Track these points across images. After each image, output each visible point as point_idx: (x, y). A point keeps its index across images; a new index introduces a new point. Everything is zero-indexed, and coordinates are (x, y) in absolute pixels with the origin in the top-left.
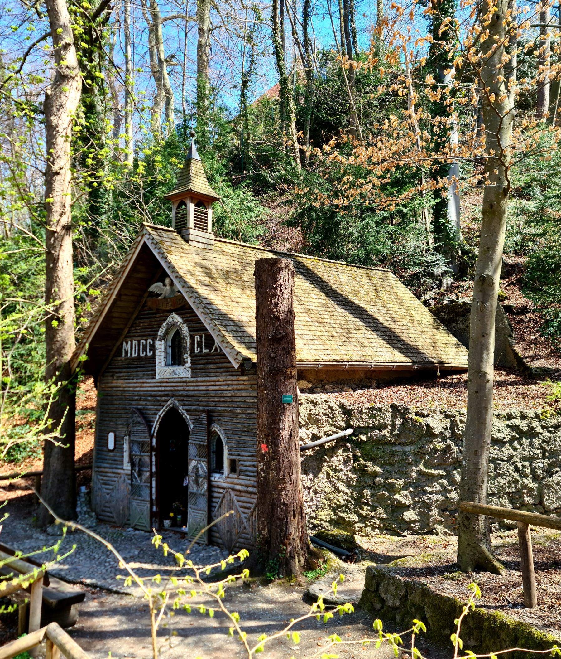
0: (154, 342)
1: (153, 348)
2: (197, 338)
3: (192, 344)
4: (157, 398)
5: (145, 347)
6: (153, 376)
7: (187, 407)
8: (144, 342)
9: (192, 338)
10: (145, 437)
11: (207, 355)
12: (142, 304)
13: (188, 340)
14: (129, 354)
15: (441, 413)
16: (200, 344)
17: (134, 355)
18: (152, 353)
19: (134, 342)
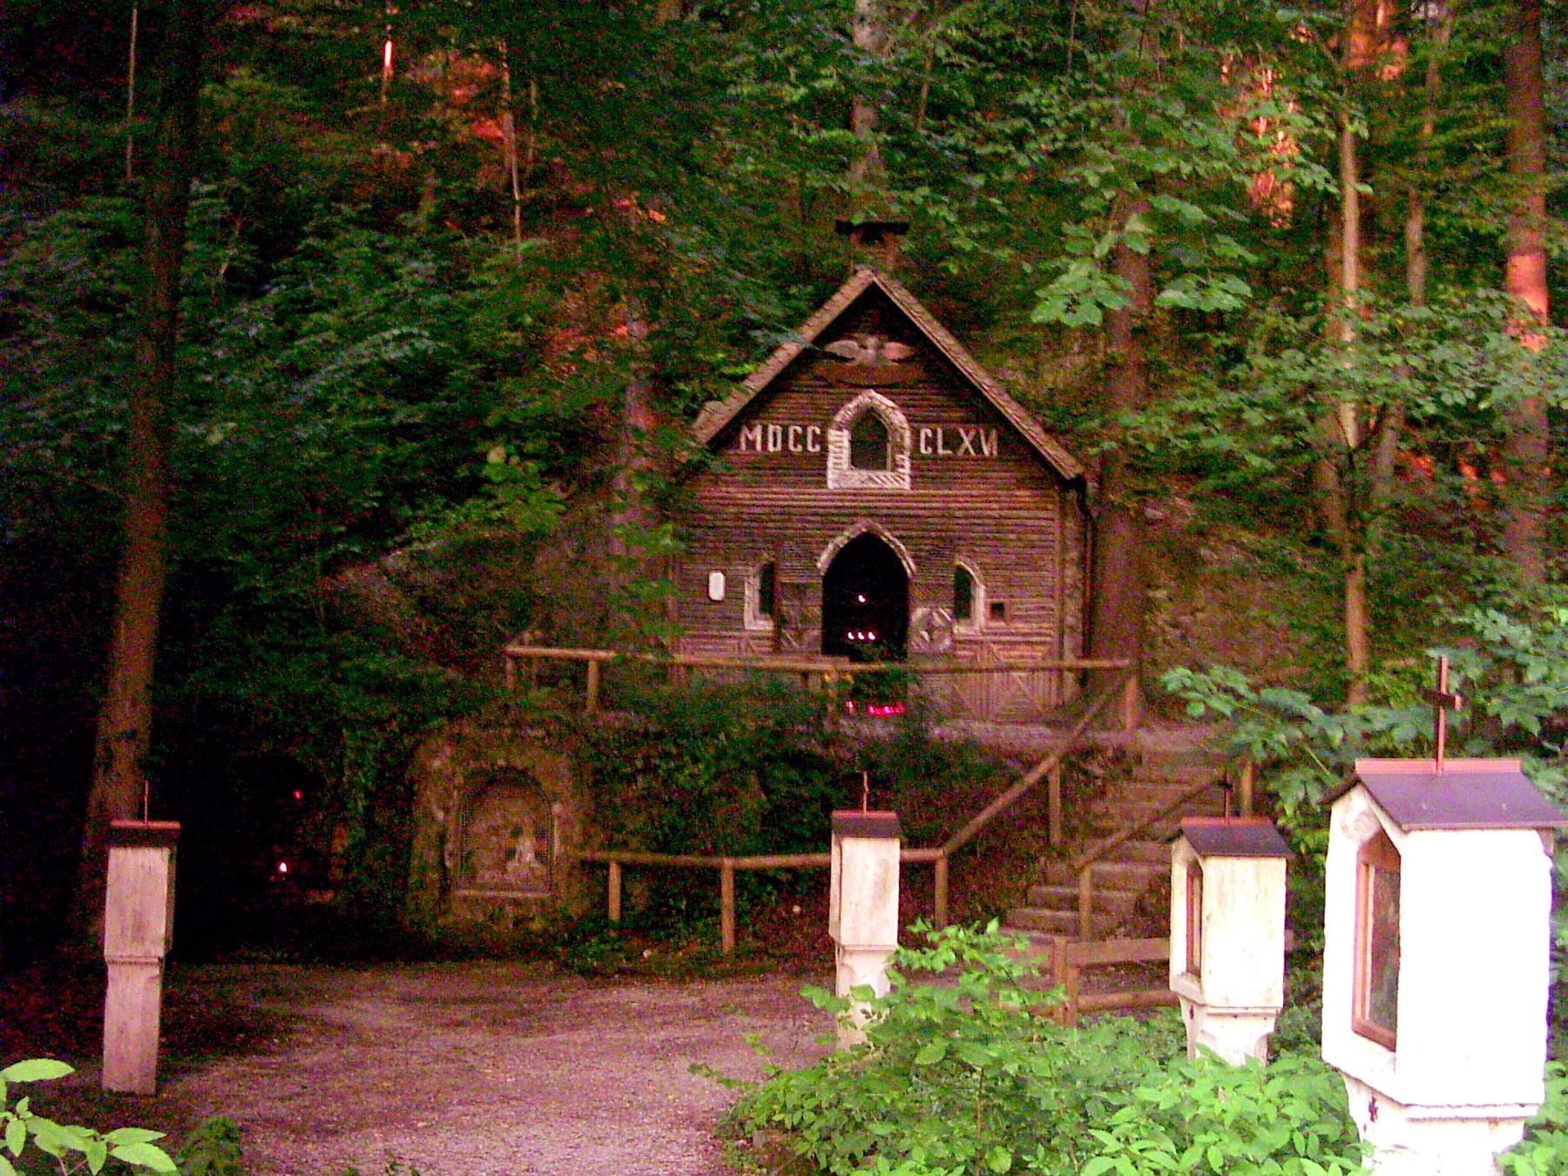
0: (824, 432)
1: (821, 440)
2: (925, 432)
3: (916, 442)
4: (830, 520)
5: (800, 439)
6: (823, 483)
7: (897, 533)
8: (799, 429)
9: (916, 433)
10: (566, 840)
11: (943, 459)
12: (739, 371)
13: (907, 434)
14: (759, 447)
15: (1149, 395)
16: (931, 442)
17: (771, 448)
18: (818, 448)
19: (771, 428)
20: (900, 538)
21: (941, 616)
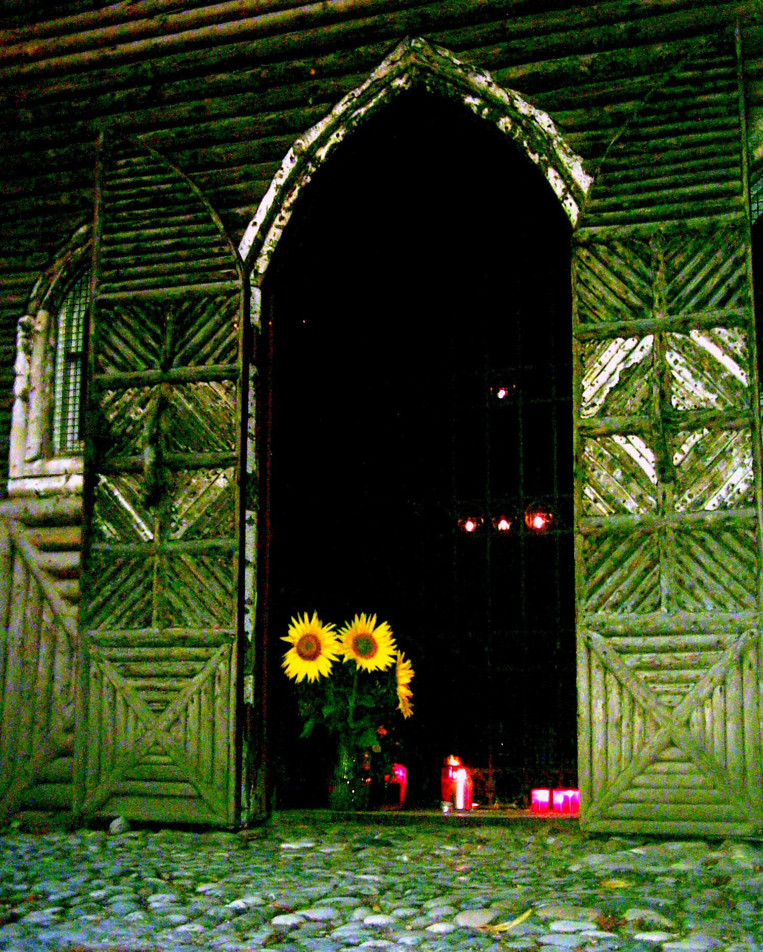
20: (529, 87)
21: (702, 364)
